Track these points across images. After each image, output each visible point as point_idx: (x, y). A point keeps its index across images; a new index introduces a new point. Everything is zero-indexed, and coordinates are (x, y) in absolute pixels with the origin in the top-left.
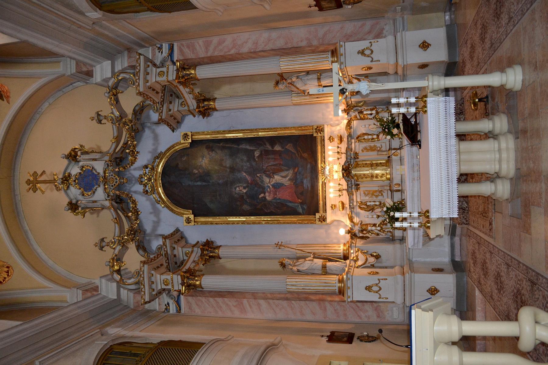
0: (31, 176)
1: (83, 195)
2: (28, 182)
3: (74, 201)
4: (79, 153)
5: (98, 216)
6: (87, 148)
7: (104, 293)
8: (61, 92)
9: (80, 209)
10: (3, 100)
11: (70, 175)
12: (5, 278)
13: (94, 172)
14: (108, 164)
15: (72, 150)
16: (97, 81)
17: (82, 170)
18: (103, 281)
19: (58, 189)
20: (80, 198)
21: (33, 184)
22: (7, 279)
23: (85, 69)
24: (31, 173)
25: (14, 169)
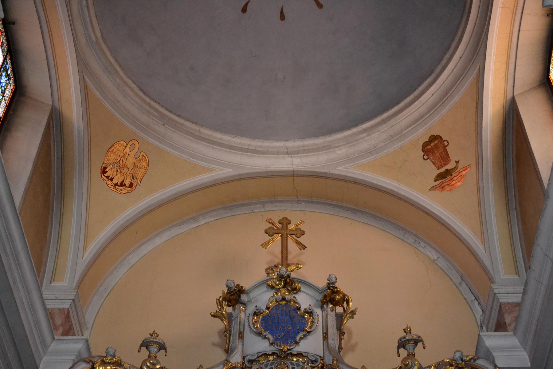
0: (296, 225)
1: (255, 314)
2: (285, 222)
3: (244, 298)
4: (339, 310)
5: (214, 344)
6: (349, 323)
7: (53, 346)
8: (460, 280)
9: (230, 310)
10: (435, 181)
11: (296, 290)
12: (112, 180)
13: (301, 335)
14: (316, 361)
15: (344, 295)
16: (485, 339)
17: (306, 312)
18: (80, 346)
19: (270, 270)
20: (251, 309)
21: (282, 230)
22: (109, 182)
23: (508, 319)
24: (302, 227)
25: (312, 202)
